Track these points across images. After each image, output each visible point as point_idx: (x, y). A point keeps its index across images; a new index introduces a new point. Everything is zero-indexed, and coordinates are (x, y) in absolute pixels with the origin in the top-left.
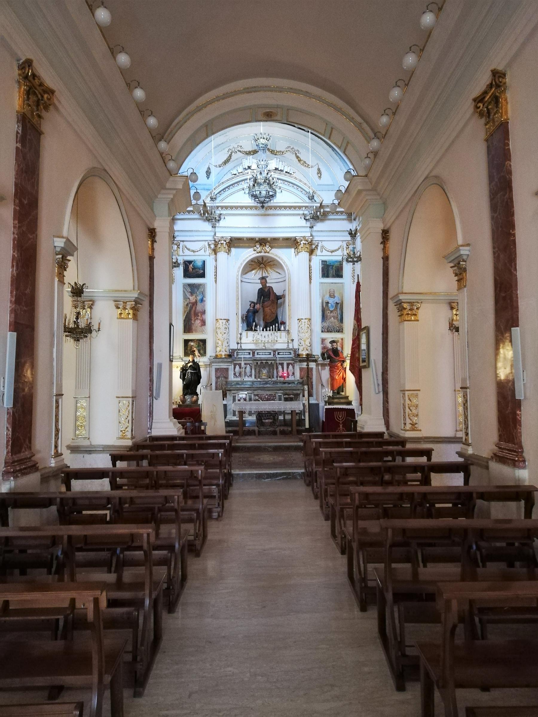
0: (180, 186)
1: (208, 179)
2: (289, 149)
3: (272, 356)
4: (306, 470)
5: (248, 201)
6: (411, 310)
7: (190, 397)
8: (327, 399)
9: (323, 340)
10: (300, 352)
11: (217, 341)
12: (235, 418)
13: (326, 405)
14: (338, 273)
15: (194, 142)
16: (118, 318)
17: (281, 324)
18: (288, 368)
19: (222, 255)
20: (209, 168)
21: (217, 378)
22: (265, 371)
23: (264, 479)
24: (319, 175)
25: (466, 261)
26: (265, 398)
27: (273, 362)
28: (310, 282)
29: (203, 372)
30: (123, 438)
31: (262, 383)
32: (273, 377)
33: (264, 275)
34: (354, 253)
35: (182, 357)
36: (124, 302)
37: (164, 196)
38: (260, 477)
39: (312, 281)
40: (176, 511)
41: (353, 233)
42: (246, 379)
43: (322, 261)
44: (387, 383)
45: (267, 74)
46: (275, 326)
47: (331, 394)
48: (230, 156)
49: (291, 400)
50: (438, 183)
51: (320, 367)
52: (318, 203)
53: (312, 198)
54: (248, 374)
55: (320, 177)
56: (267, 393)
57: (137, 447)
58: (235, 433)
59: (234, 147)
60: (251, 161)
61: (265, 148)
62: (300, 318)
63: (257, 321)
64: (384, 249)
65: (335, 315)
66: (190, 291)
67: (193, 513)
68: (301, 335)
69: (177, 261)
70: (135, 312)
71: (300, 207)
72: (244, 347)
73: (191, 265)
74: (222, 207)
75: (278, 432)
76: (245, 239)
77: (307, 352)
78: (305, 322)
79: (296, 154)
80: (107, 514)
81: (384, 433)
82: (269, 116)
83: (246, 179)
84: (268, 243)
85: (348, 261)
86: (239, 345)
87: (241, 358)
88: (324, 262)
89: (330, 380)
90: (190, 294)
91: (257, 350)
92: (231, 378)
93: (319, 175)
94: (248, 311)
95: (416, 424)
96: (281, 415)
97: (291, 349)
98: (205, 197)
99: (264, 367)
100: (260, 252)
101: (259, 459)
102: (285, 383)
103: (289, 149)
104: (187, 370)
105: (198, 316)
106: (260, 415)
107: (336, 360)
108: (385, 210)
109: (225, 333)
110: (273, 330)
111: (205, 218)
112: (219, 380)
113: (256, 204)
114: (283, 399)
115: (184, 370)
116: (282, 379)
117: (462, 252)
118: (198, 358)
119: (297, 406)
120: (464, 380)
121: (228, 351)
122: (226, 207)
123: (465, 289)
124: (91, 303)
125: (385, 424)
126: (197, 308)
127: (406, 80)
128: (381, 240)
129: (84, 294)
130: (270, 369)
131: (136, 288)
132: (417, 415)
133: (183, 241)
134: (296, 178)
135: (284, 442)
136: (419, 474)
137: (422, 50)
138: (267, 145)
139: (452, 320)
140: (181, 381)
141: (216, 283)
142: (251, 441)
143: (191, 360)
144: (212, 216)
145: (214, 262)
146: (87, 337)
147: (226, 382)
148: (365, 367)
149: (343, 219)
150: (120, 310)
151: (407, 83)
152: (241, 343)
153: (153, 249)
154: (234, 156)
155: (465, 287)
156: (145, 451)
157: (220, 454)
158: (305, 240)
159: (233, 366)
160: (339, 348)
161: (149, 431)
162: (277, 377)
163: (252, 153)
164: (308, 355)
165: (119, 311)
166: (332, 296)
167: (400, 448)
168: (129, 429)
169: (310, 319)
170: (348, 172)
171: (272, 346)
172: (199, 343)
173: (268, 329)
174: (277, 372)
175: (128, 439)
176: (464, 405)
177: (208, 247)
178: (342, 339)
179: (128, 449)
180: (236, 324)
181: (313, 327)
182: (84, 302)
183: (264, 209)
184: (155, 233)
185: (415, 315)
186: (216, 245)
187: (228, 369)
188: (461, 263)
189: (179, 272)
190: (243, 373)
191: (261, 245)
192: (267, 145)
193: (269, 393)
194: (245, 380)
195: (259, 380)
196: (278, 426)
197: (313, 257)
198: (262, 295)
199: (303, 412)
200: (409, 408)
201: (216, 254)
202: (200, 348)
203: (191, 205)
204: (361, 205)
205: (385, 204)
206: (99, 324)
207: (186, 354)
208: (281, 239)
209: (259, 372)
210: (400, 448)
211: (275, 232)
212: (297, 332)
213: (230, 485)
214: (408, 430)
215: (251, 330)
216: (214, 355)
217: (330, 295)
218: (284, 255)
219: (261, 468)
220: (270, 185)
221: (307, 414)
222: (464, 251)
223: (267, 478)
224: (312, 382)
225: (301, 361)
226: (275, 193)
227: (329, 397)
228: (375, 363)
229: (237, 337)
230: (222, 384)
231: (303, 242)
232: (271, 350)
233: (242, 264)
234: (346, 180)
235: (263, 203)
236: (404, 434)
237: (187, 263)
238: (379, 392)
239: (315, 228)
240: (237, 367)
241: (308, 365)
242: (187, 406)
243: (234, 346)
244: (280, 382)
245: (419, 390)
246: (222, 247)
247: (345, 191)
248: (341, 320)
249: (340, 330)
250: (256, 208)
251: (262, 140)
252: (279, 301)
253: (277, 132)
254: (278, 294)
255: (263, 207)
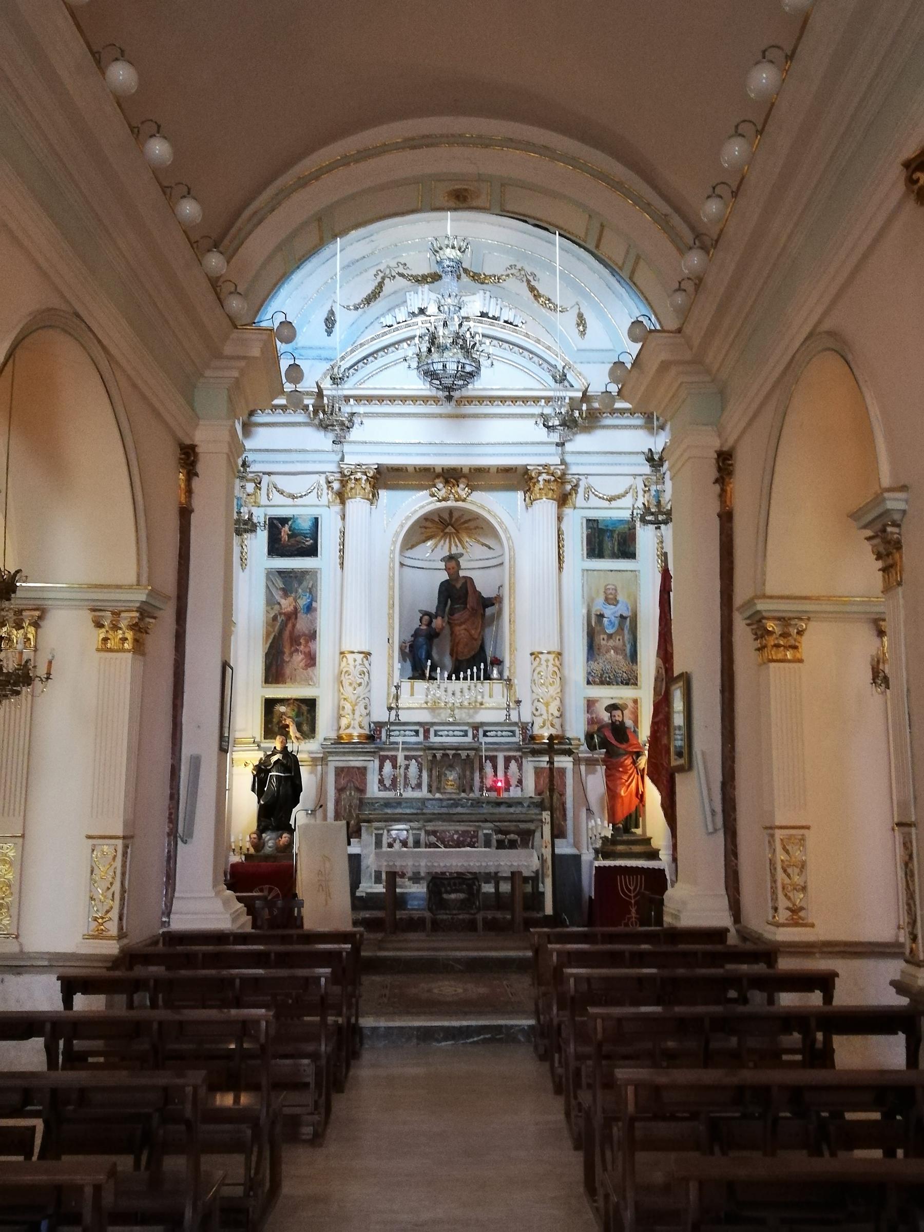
0: (256, 352)
1: (329, 334)
2: (513, 271)
3: (469, 739)
4: (538, 1020)
5: (418, 386)
6: (785, 635)
7: (274, 835)
8: (599, 845)
9: (590, 704)
10: (537, 731)
11: (342, 702)
12: (380, 889)
13: (596, 859)
14: (625, 546)
15: (293, 255)
16: (98, 650)
17: (492, 664)
18: (507, 767)
19: (357, 506)
20: (332, 312)
21: (340, 790)
22: (452, 776)
23: (440, 1042)
24: (581, 328)
25: (899, 526)
26: (453, 840)
27: (472, 753)
28: (560, 568)
29: (307, 776)
30: (99, 935)
31: (445, 803)
32: (472, 790)
33: (454, 551)
34: (659, 502)
35: (258, 739)
36: (113, 613)
37: (220, 373)
38: (427, 1034)
39: (564, 565)
40: (188, 1123)
41: (656, 457)
42: (409, 794)
43: (588, 521)
44: (734, 809)
45: (456, 109)
46: (479, 670)
47: (608, 832)
48: (380, 286)
49: (512, 845)
50: (838, 346)
51: (583, 768)
52: (577, 390)
53: (561, 379)
54: (413, 782)
55: (583, 333)
56: (458, 828)
57: (130, 958)
58: (371, 925)
59: (388, 267)
60: (425, 297)
61: (459, 270)
62: (536, 649)
63: (435, 656)
64: (723, 495)
65: (619, 644)
66: (282, 586)
67: (243, 1127)
68: (539, 691)
69: (250, 519)
70: (139, 634)
71: (536, 400)
72: (404, 717)
73: (286, 528)
74: (358, 399)
75: (480, 925)
76: (411, 470)
77: (553, 732)
78: (547, 661)
79: (528, 281)
80: (34, 1128)
81: (727, 930)
82: (461, 199)
83: (413, 338)
84: (463, 480)
85: (644, 521)
86: (393, 712)
87: (397, 743)
88: (592, 524)
89: (606, 797)
90: (281, 593)
91: (433, 724)
92: (373, 790)
93: (581, 328)
94: (416, 634)
95: (802, 909)
96: (487, 882)
97: (516, 724)
98: (314, 375)
99: (451, 767)
100: (445, 499)
101: (429, 991)
102: (498, 804)
103: (513, 271)
104: (270, 771)
105: (300, 644)
106: (438, 883)
107: (622, 751)
108: (723, 409)
109: (360, 684)
110: (472, 679)
111: (317, 422)
112: (343, 796)
113: (434, 392)
114: (494, 843)
115: (261, 771)
116: (493, 795)
117: (890, 505)
118: (296, 744)
119: (526, 861)
120: (903, 806)
121: (367, 727)
122: (369, 399)
123: (900, 589)
124: (37, 613)
125: (731, 908)
126: (298, 626)
127: (759, 121)
128: (713, 474)
129: (19, 594)
130: (464, 771)
131: (144, 580)
132: (804, 889)
133: (269, 474)
134: (527, 335)
135: (502, 949)
136: (796, 1036)
137: (790, 57)
138: (459, 262)
139: (878, 662)
140: (255, 797)
141: (342, 568)
142: (414, 946)
143: (278, 748)
144: (334, 417)
145: (340, 523)
146: (18, 693)
147: (361, 800)
148: (681, 769)
149: (635, 427)
150: (104, 630)
151: (759, 128)
152: (398, 708)
153: (189, 491)
154: (389, 286)
155: (899, 584)
156: (156, 970)
157: (323, 980)
158: (548, 473)
159: (377, 762)
160: (629, 723)
161: (164, 919)
162: (481, 790)
163: (429, 280)
164: (551, 738)
165: (102, 634)
166: (611, 600)
167: (760, 968)
168: (114, 914)
169: (560, 654)
170: (637, 323)
171: (471, 716)
172: (299, 708)
173: (462, 675)
174: (481, 778)
175: (111, 938)
176: (906, 865)
177: (325, 486)
178: (635, 701)
179: (110, 965)
180: (387, 665)
181: (566, 672)
182: (19, 612)
183: (453, 403)
184: (196, 455)
185: (795, 648)
186: (343, 483)
187: (365, 768)
188: (889, 529)
189: (259, 541)
190: (401, 780)
191: (447, 482)
192: (459, 262)
193: (461, 828)
194: (405, 795)
195: (438, 795)
196: (479, 909)
197: (568, 511)
198: (449, 597)
199: (536, 879)
200: (785, 871)
201: (343, 502)
202: (300, 719)
203: (282, 392)
204: (670, 395)
205: (722, 395)
206: (50, 663)
207: (269, 733)
208: (493, 470)
209: (439, 777)
210: (760, 968)
211: (479, 455)
212: (529, 681)
213: (355, 1055)
214: (783, 925)
215: (422, 677)
216: (333, 735)
217: (607, 599)
218: (495, 505)
219: (431, 1014)
220: (467, 350)
221: (549, 881)
222: (895, 502)
223: (446, 1039)
224: (563, 804)
225: (535, 753)
226: (478, 368)
227: (605, 839)
228: (705, 763)
229: (388, 694)
230: (350, 806)
231: (545, 476)
232: (468, 724)
233: (402, 526)
234: (634, 338)
235: (449, 389)
236: (775, 934)
237: (275, 525)
238: (716, 830)
239: (569, 447)
240: (388, 765)
241: (551, 762)
242: (267, 857)
243: (380, 714)
244: (488, 803)
245: (808, 828)
246: (358, 487)
247: (633, 365)
248: (634, 657)
249: (631, 680)
250: (436, 400)
251: (448, 250)
252: (489, 611)
253: (489, 236)
254: (485, 595)
255: (449, 398)
